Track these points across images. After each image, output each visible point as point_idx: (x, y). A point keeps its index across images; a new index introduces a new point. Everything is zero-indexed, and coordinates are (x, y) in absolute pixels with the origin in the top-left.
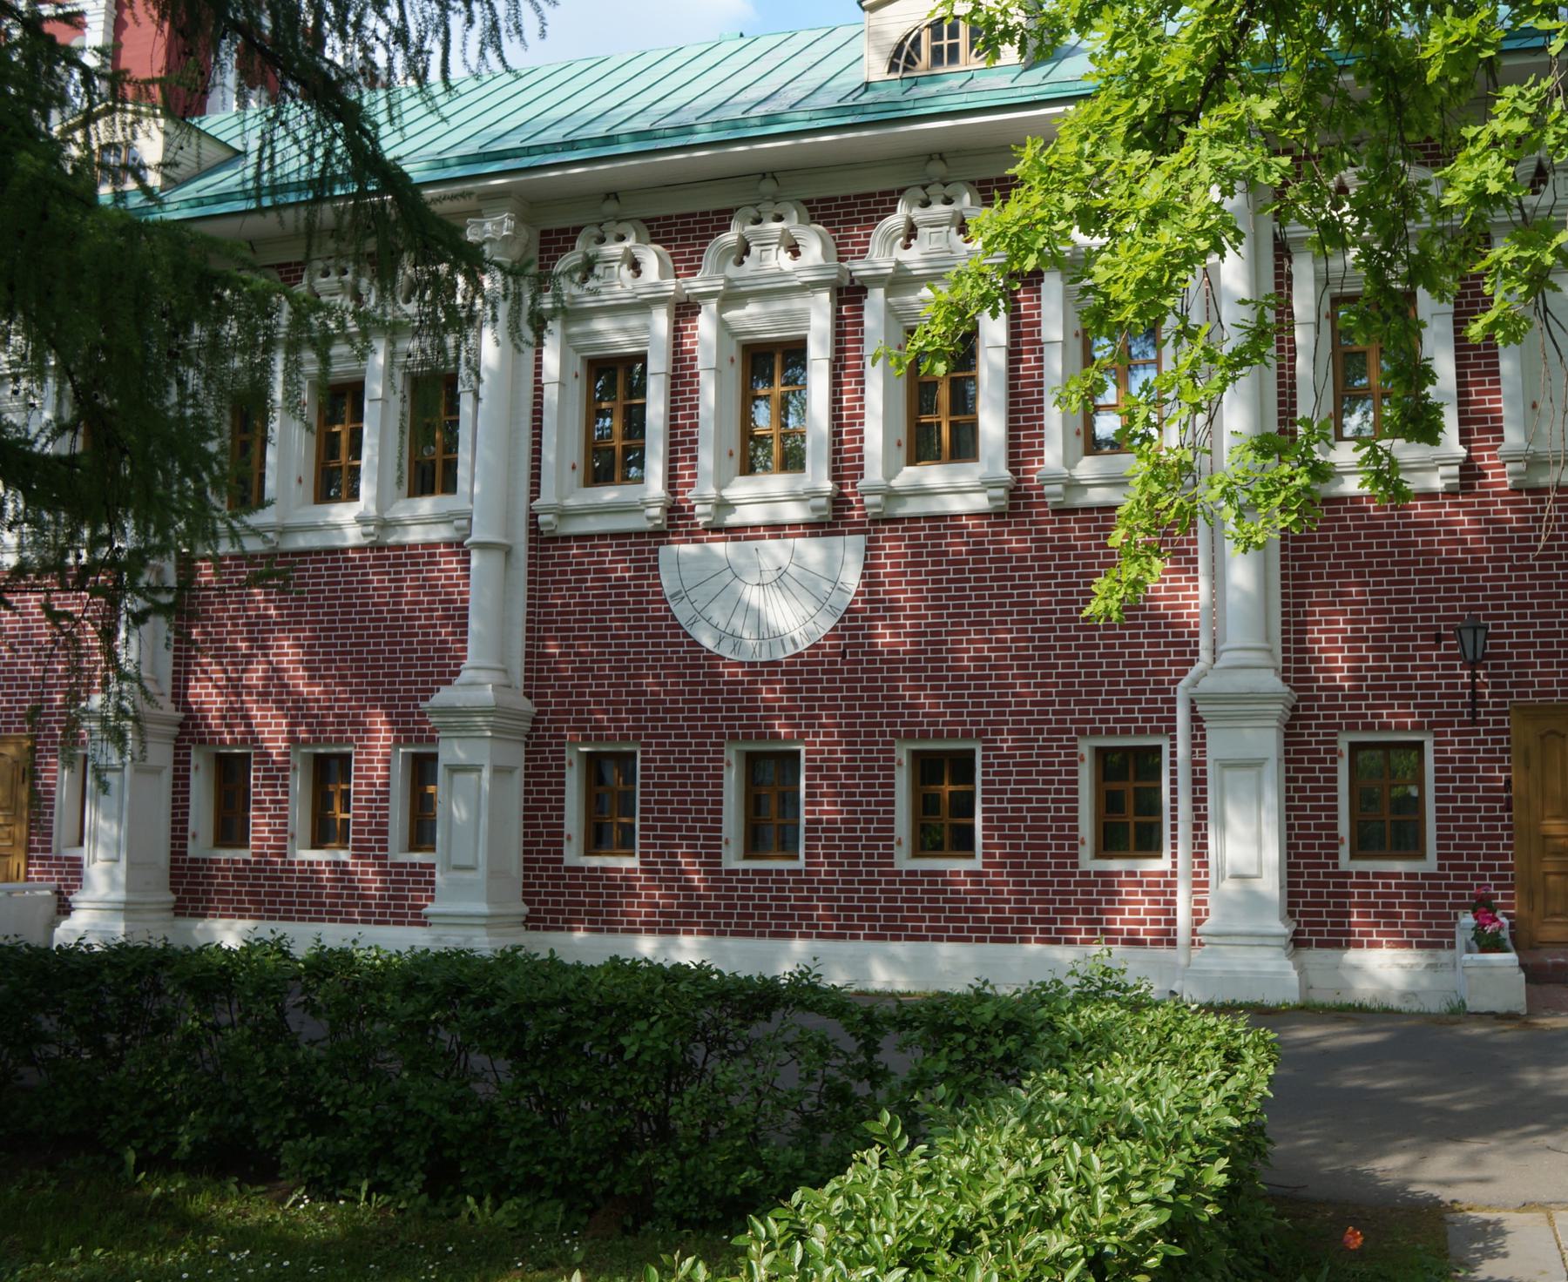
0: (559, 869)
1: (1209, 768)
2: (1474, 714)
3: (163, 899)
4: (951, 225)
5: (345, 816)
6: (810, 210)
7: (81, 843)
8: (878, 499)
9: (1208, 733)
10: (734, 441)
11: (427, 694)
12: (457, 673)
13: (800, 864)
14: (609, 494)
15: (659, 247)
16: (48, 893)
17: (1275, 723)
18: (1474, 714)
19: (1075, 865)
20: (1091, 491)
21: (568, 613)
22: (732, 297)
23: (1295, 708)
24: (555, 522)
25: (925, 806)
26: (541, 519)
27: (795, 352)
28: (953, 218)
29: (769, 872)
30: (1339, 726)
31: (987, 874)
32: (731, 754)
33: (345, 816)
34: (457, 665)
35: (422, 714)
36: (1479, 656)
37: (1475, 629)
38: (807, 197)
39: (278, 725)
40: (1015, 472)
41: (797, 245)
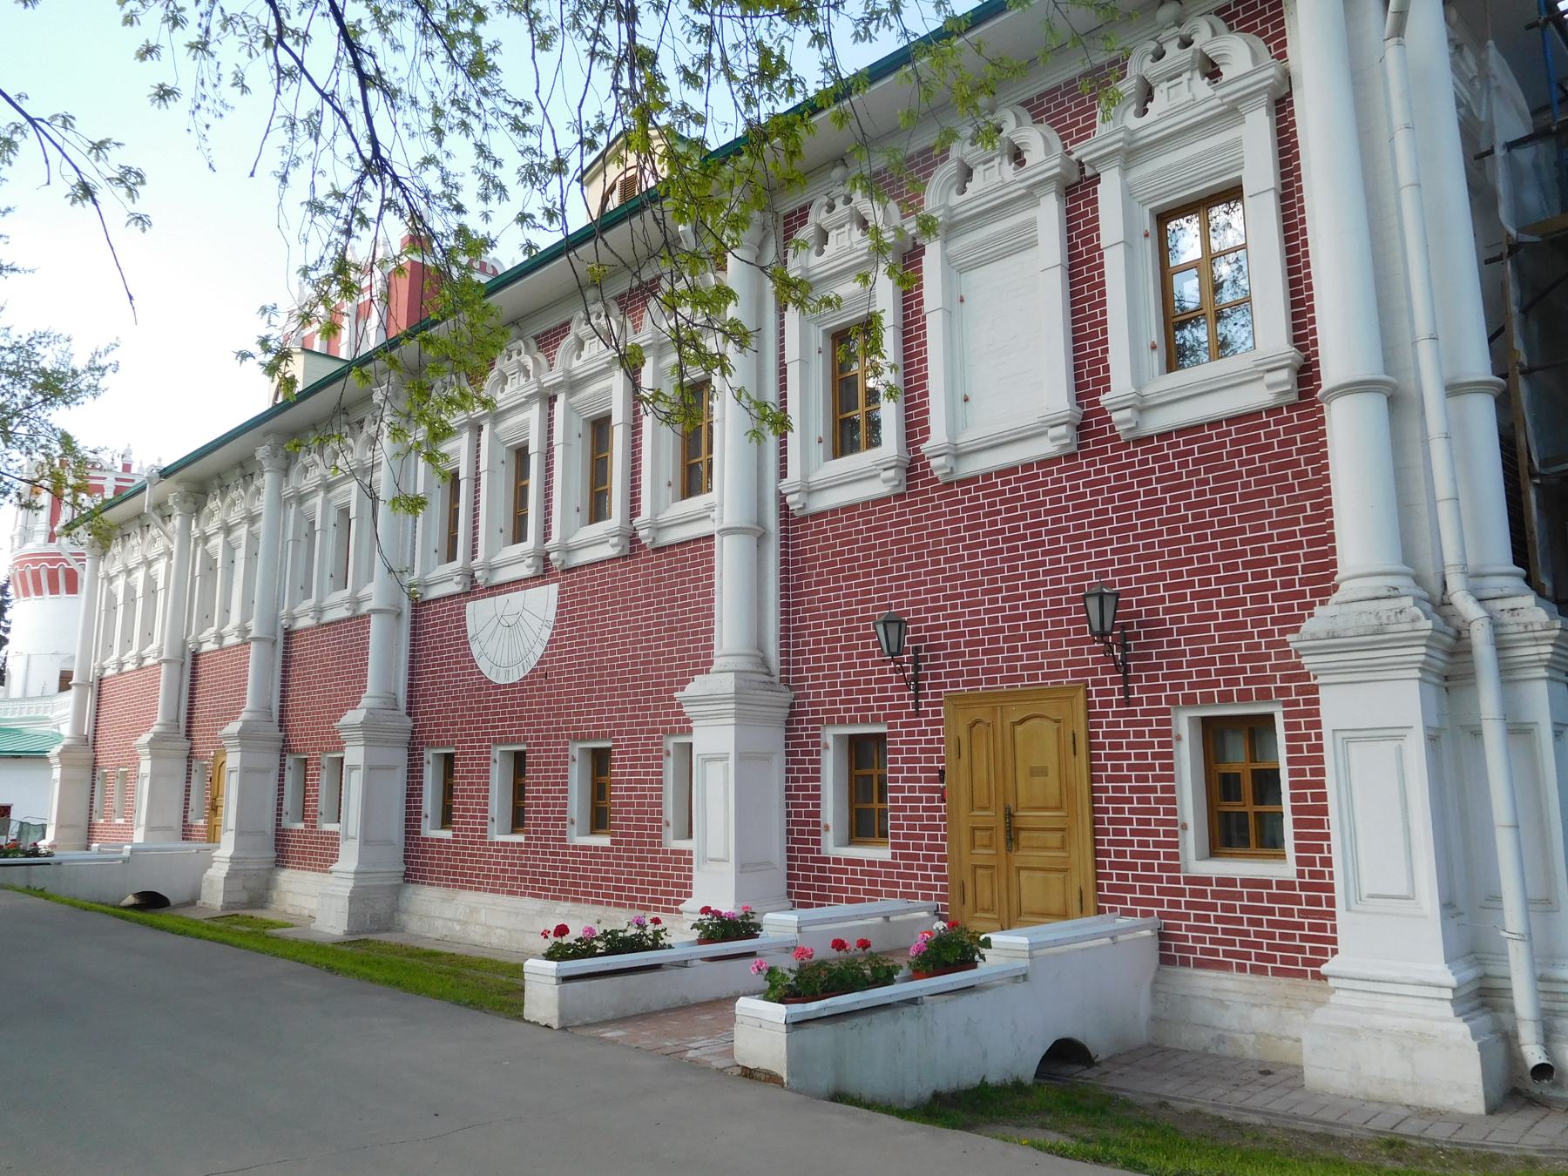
0: (1177, 880)
1: (1327, 742)
2: (917, 705)
3: (394, 869)
4: (1193, 70)
5: (882, 806)
6: (1226, 20)
7: (690, 836)
8: (1127, 414)
9: (1323, 694)
10: (1152, 330)
11: (337, 718)
12: (711, 663)
13: (1285, 869)
14: (697, 503)
15: (1044, 127)
16: (1147, 933)
17: (1543, 672)
18: (917, 705)
19: (660, 844)
20: (580, 553)
21: (863, 584)
22: (1131, 154)
23: (792, 706)
24: (951, 463)
25: (1221, 786)
26: (789, 499)
27: (869, 325)
28: (851, 215)
29: (860, 862)
30: (821, 721)
31: (897, 866)
32: (497, 752)
33: (882, 806)
34: (708, 655)
35: (680, 705)
36: (1108, 626)
37: (1101, 596)
38: (1026, 97)
39: (901, 698)
40: (1302, 348)
41: (1214, 65)
